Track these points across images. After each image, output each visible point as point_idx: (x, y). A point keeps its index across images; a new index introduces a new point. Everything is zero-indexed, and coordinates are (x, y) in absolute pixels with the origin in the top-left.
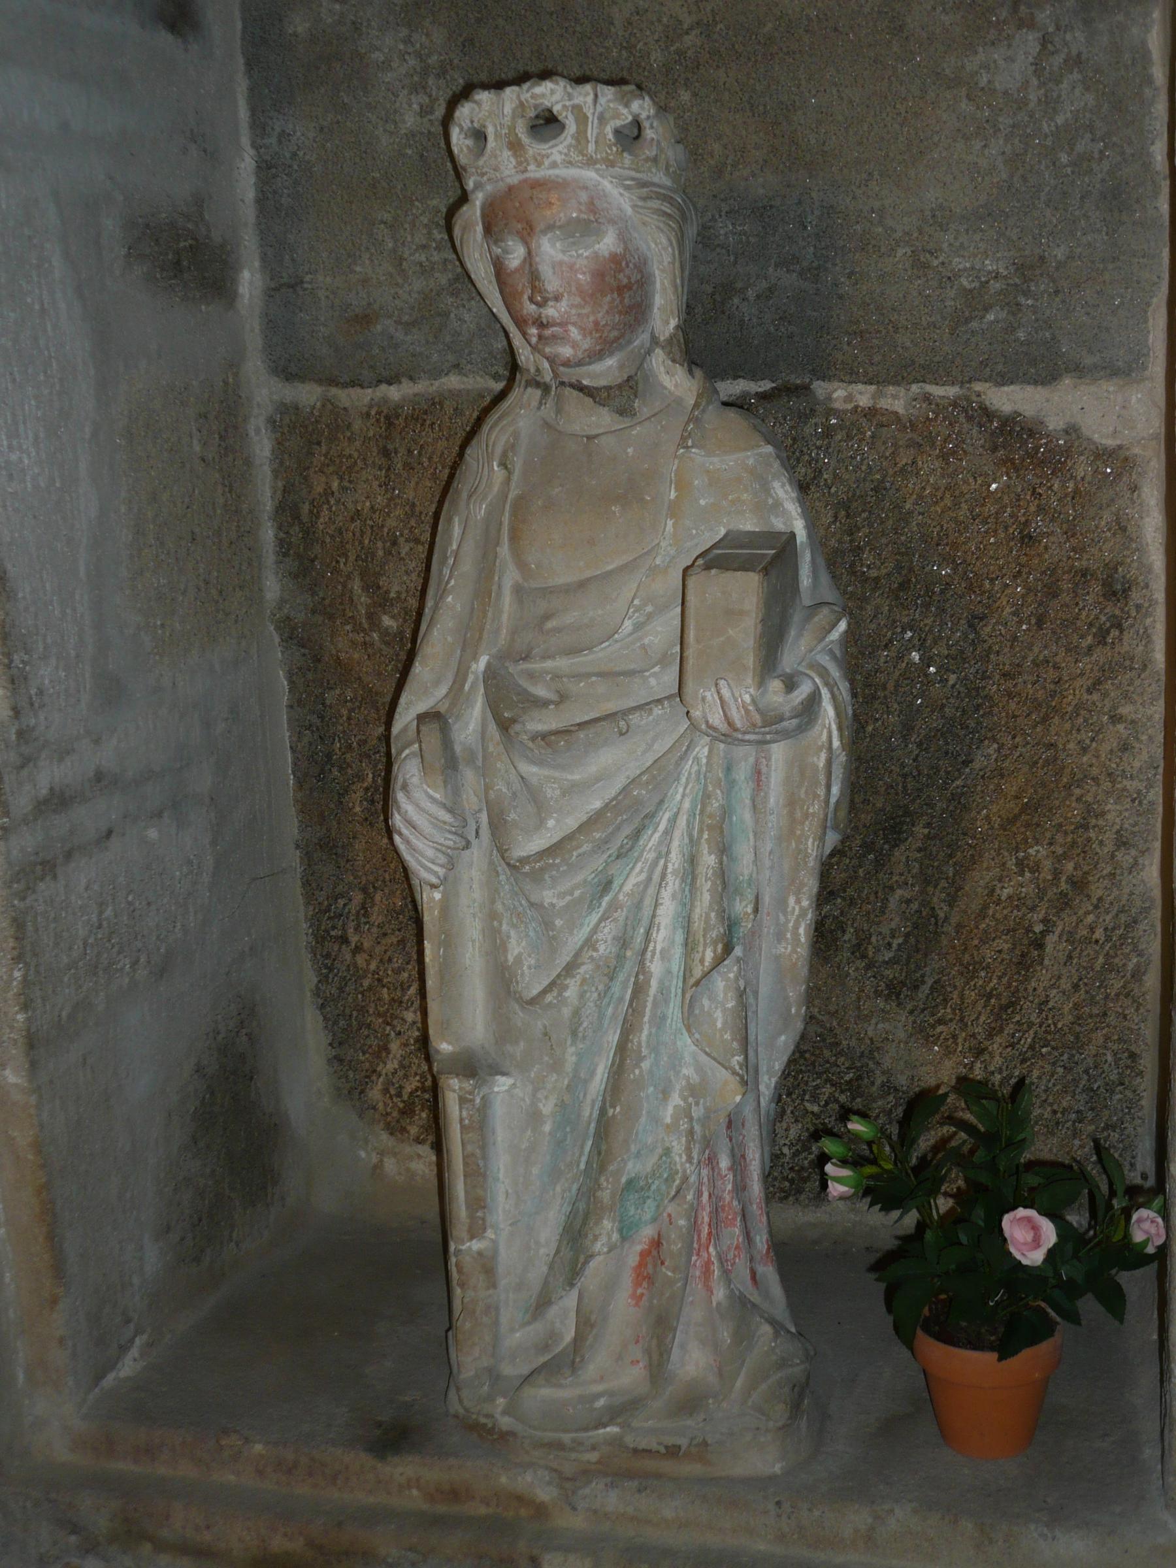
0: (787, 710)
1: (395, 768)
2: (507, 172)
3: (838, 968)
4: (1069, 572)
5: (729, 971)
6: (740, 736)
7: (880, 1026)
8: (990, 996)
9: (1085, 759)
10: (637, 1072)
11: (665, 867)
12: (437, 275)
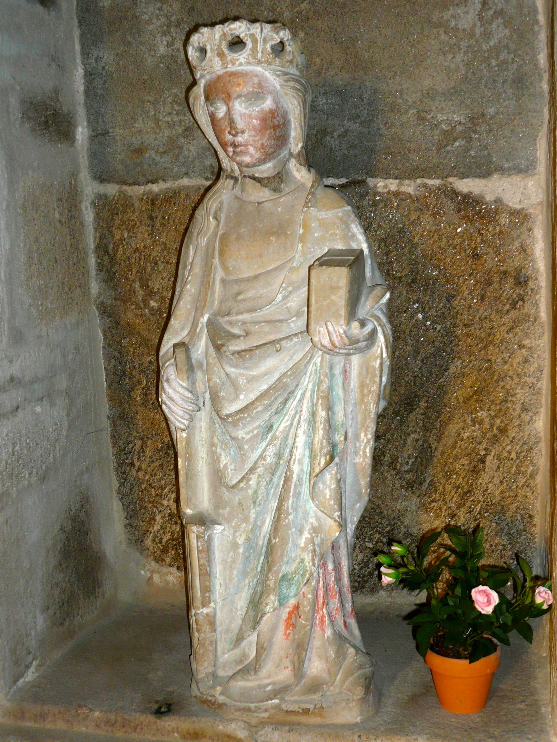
0: (361, 337)
1: (162, 372)
2: (217, 69)
3: (382, 474)
4: (497, 273)
5: (332, 470)
6: (337, 351)
7: (403, 503)
8: (458, 487)
9: (506, 367)
10: (287, 521)
11: (300, 418)
12: (176, 128)
